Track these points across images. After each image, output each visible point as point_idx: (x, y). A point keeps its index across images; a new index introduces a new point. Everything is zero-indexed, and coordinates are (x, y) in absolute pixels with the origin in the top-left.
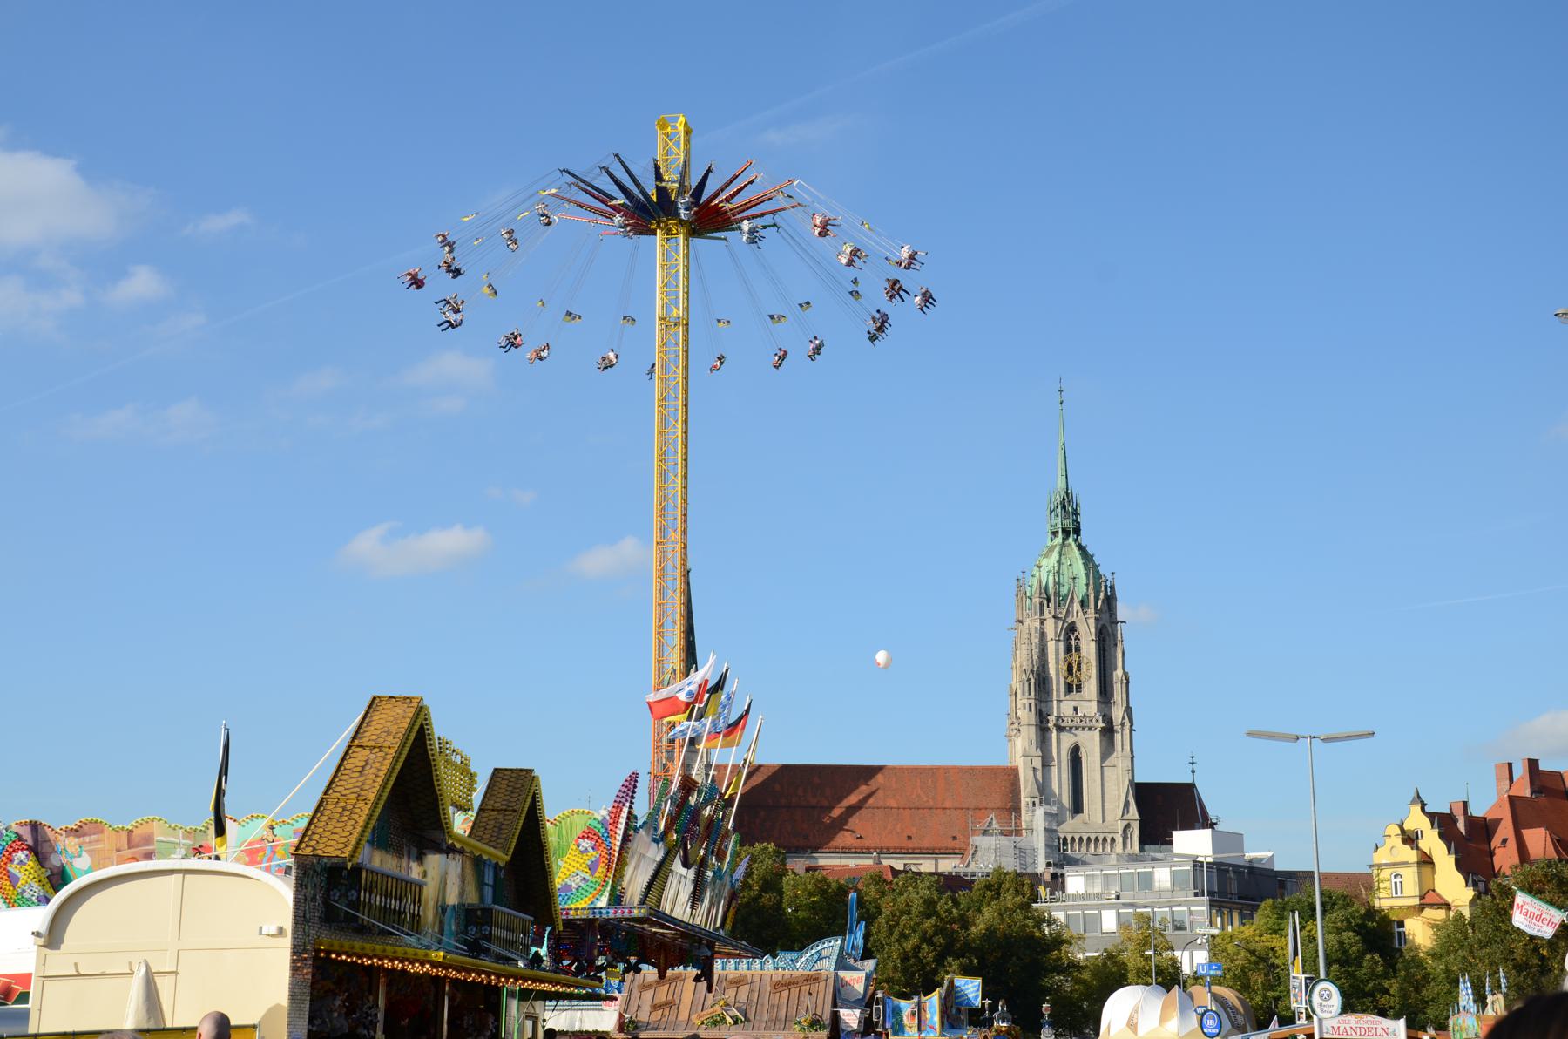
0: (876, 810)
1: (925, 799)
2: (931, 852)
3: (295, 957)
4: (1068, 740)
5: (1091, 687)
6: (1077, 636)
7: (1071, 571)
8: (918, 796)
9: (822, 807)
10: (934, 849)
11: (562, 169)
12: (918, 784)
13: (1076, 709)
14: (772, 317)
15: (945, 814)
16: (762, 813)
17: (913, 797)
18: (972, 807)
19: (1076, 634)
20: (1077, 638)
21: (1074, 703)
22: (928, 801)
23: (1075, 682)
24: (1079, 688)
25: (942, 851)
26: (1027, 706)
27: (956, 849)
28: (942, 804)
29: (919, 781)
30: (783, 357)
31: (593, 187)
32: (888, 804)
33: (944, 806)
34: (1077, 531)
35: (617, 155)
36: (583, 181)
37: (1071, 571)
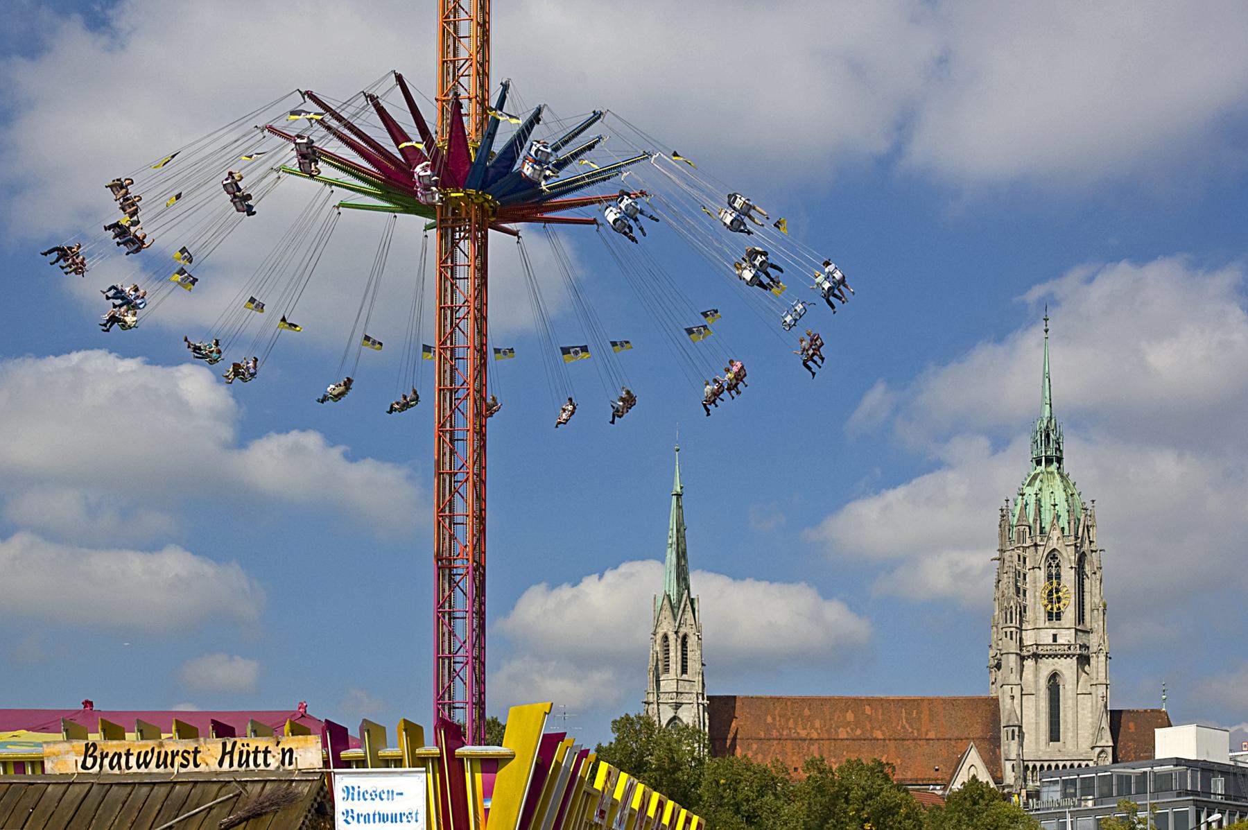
0: (863, 741)
1: (910, 730)
2: (914, 783)
3: (393, 766)
4: (1047, 666)
5: (1069, 615)
6: (1058, 564)
7: (1053, 498)
8: (903, 727)
9: (811, 739)
10: (917, 781)
11: (303, 91)
12: (904, 714)
13: (1055, 636)
14: (614, 344)
15: (928, 744)
16: (755, 746)
17: (899, 728)
18: (955, 737)
19: (1057, 561)
20: (1058, 565)
21: (1054, 631)
22: (912, 732)
23: (1055, 610)
24: (1059, 618)
25: (925, 782)
26: (1009, 634)
27: (938, 779)
28: (927, 734)
29: (903, 710)
30: (629, 401)
31: (351, 128)
32: (874, 736)
33: (927, 737)
34: (1059, 460)
35: (399, 79)
36: (339, 118)
37: (1053, 498)
